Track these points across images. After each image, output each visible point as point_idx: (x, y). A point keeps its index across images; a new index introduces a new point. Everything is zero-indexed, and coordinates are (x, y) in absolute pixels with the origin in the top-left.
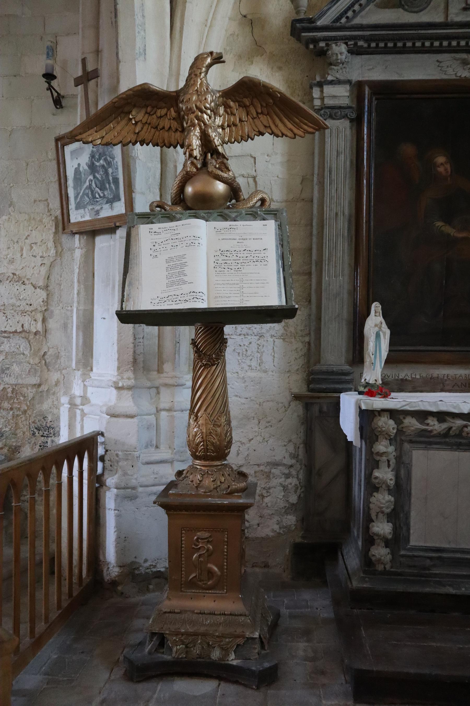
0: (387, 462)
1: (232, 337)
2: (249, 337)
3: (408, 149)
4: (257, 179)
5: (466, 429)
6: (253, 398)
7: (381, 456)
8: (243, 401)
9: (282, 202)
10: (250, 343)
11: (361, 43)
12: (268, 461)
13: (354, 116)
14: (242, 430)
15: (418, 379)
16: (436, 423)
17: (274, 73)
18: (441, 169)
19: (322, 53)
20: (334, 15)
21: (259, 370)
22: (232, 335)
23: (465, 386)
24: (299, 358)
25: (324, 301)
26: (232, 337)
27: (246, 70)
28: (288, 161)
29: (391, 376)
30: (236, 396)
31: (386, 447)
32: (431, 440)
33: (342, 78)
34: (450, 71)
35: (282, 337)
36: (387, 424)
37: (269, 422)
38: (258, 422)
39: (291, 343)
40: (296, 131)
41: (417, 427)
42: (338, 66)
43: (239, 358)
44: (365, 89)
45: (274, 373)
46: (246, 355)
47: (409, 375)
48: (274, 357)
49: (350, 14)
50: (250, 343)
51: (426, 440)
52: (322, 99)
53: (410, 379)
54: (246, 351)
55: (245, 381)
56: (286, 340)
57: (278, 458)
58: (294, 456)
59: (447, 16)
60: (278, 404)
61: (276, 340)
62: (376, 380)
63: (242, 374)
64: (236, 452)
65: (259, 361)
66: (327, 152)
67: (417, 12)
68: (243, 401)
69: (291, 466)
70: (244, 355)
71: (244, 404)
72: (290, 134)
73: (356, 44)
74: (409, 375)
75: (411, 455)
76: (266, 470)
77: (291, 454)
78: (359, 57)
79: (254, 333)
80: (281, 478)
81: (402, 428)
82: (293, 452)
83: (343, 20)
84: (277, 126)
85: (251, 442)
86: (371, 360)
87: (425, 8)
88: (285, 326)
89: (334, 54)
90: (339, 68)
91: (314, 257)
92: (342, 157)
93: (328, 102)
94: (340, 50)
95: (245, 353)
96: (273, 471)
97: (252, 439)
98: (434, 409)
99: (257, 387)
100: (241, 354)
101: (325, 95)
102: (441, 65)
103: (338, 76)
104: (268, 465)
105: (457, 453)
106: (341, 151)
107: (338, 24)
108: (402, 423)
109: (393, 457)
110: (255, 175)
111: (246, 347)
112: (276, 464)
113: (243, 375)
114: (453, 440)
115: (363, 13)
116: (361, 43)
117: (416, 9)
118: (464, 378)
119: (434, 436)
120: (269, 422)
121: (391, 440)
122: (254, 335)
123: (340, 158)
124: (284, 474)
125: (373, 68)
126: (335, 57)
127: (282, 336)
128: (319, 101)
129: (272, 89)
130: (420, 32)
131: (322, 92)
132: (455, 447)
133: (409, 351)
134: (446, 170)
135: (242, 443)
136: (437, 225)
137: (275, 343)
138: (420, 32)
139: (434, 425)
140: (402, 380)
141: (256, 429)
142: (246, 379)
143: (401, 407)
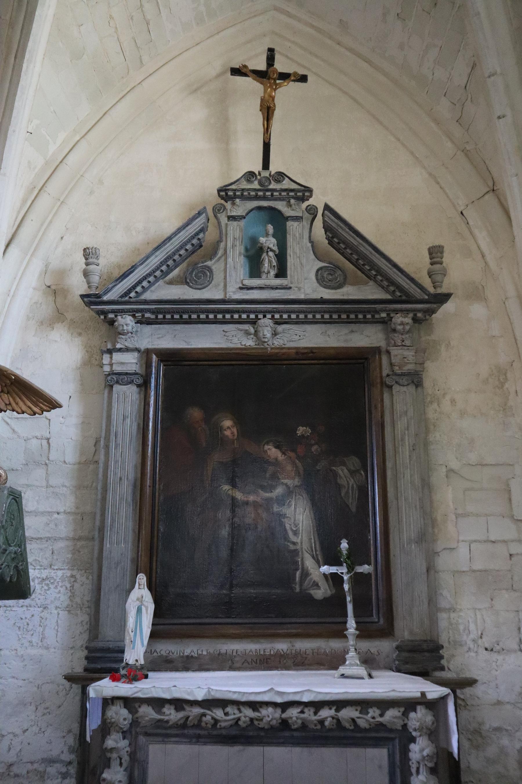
0: (118, 760)
1: (14, 609)
2: (32, 609)
3: (195, 414)
4: (50, 441)
5: (204, 719)
6: (31, 680)
7: (111, 753)
8: (21, 683)
9: (74, 464)
10: (33, 616)
11: (147, 315)
12: (43, 757)
13: (140, 381)
14: (17, 719)
15: (205, 655)
16: (173, 711)
17: (73, 339)
18: (228, 433)
19: (112, 322)
20: (121, 291)
21: (40, 647)
22: (13, 606)
23: (256, 663)
24: (85, 632)
25: (104, 570)
26: (14, 609)
27: (47, 336)
28: (83, 423)
29: (176, 653)
30: (13, 677)
31: (117, 742)
32: (169, 732)
33: (131, 346)
34: (235, 340)
35: (67, 609)
36: (120, 715)
37: (47, 708)
38: (35, 708)
39: (77, 615)
40: (35, 409)
41: (152, 717)
42: (126, 335)
43: (19, 633)
44: (152, 358)
45: (56, 650)
46: (27, 630)
47: (195, 651)
48: (57, 631)
49: (139, 289)
50: (33, 616)
51: (162, 732)
52: (111, 365)
53: (196, 655)
54: (28, 624)
55: (24, 660)
56: (72, 612)
57: (55, 753)
58: (71, 750)
59: (226, 294)
60: (59, 686)
61: (60, 612)
62: (137, 661)
63: (21, 652)
64: (7, 747)
65: (41, 636)
66: (114, 417)
67: (200, 289)
68: (21, 683)
69: (70, 763)
70: (25, 630)
71: (21, 687)
72: (29, 411)
73: (143, 316)
74: (195, 651)
75: (148, 752)
76: (40, 769)
77: (70, 747)
78: (149, 327)
79: (37, 604)
80: (57, 778)
81: (137, 718)
82: (73, 745)
83: (133, 294)
84: (17, 404)
85: (26, 734)
86: (131, 638)
87: (207, 286)
88: (71, 596)
89: (120, 325)
90: (127, 337)
91: (98, 523)
92: (128, 421)
93: (117, 368)
94: (126, 322)
95: (25, 627)
96: (49, 769)
97: (27, 730)
98: (167, 696)
99: (37, 666)
100: (22, 628)
101: (113, 362)
102: (227, 334)
103: (127, 345)
104: (42, 762)
105: (197, 746)
106: (127, 414)
107: (127, 298)
108: (137, 712)
109: (126, 753)
110: (48, 437)
111: (27, 620)
112: (50, 761)
113: (22, 653)
114: (191, 732)
115: (153, 288)
116: (147, 315)
117: (199, 287)
118: (254, 654)
119: (171, 727)
120: (47, 708)
121: (123, 732)
122: (37, 606)
123: (126, 422)
124: (61, 773)
125: (162, 337)
126: (121, 328)
127: (67, 607)
128: (109, 366)
129: (6, 371)
130: (201, 306)
131: (111, 358)
132: (194, 740)
133: (193, 624)
134: (232, 433)
135: (15, 735)
136: (224, 489)
137: (60, 616)
138: (201, 306)
139: (170, 714)
140: (187, 656)
141: (33, 717)
142: (25, 657)
143: (132, 695)
